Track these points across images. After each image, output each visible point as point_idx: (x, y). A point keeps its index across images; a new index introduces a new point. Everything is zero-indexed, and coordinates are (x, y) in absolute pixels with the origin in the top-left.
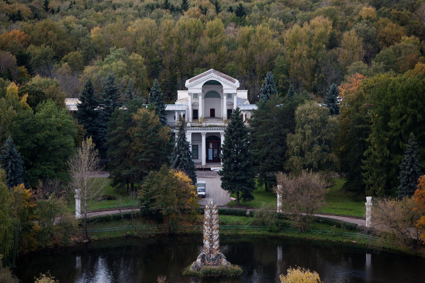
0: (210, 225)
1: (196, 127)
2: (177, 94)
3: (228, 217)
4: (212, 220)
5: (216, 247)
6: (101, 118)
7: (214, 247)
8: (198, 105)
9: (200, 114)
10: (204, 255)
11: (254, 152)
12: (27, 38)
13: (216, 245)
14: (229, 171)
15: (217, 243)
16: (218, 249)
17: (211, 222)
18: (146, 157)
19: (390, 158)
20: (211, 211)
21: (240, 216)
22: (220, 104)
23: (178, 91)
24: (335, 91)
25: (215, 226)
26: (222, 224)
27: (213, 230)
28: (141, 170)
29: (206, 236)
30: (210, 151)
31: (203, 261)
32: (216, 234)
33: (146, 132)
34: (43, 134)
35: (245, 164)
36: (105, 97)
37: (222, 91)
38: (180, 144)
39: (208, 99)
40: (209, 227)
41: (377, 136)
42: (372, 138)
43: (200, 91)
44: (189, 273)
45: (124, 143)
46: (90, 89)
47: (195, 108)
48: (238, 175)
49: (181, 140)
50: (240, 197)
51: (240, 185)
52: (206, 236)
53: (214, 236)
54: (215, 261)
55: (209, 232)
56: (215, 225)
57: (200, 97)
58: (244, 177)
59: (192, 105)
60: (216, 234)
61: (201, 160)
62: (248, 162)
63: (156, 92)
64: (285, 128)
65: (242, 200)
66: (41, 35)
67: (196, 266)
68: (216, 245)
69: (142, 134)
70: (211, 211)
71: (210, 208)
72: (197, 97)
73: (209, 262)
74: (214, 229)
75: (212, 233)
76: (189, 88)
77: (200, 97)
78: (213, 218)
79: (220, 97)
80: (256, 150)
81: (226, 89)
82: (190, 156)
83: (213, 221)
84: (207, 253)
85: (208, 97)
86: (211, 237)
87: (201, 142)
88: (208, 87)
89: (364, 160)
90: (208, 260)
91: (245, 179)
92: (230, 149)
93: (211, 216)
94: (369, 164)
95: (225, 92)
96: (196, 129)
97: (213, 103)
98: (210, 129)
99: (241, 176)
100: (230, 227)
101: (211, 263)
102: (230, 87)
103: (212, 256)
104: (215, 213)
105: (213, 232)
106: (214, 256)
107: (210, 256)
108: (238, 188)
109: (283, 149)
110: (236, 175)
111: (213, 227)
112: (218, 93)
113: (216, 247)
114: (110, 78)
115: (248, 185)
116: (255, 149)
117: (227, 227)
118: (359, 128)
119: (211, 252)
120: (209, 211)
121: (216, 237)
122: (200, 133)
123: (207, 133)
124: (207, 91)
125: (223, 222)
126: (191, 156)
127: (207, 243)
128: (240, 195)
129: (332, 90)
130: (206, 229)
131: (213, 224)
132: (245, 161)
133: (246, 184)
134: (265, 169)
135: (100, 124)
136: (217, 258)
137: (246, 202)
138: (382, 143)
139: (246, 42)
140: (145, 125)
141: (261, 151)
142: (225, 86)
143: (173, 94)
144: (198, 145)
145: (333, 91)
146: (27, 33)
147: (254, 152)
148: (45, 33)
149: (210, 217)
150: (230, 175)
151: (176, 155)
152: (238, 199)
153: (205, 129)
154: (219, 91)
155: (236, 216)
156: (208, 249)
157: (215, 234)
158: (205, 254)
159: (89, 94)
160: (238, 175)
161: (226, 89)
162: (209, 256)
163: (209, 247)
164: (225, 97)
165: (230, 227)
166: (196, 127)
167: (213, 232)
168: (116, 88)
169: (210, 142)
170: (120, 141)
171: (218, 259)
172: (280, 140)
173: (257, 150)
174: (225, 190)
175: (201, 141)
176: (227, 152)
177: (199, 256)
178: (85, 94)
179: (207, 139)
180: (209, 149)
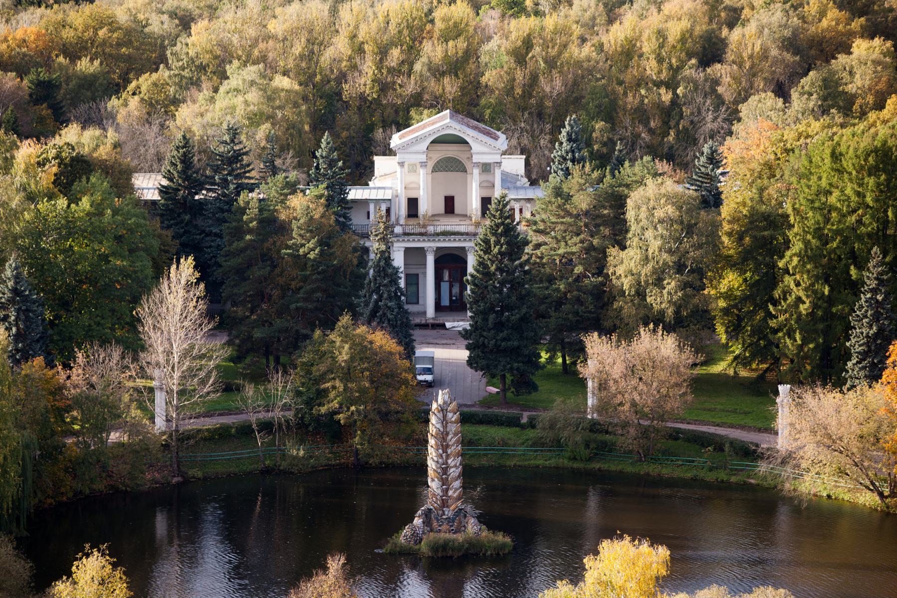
3: (481, 428)
4: (447, 434)
5: (454, 492)
7: (450, 493)
13: (456, 489)
15: (457, 484)
21: (507, 426)
25: (453, 448)
27: (448, 457)
39: (432, 356)
44: (398, 549)
48: (504, 339)
53: (452, 470)
54: (453, 522)
56: (453, 445)
58: (516, 343)
61: (425, 305)
75: (447, 463)
76: (400, 151)
78: (448, 430)
81: (478, 153)
82: (400, 297)
83: (450, 437)
84: (436, 505)
86: (445, 471)
90: (438, 520)
91: (518, 347)
95: (476, 159)
99: (509, 340)
100: (485, 450)
103: (446, 513)
104: (453, 419)
105: (449, 461)
111: (449, 451)
113: (454, 492)
117: (479, 450)
119: (444, 504)
121: (454, 472)
123: (438, 249)
126: (403, 298)
136: (457, 516)
142: (475, 147)
144: (417, 275)
151: (371, 296)
154: (463, 157)
161: (478, 153)
165: (485, 450)
167: (449, 461)
171: (460, 519)
175: (425, 265)
179: (437, 262)
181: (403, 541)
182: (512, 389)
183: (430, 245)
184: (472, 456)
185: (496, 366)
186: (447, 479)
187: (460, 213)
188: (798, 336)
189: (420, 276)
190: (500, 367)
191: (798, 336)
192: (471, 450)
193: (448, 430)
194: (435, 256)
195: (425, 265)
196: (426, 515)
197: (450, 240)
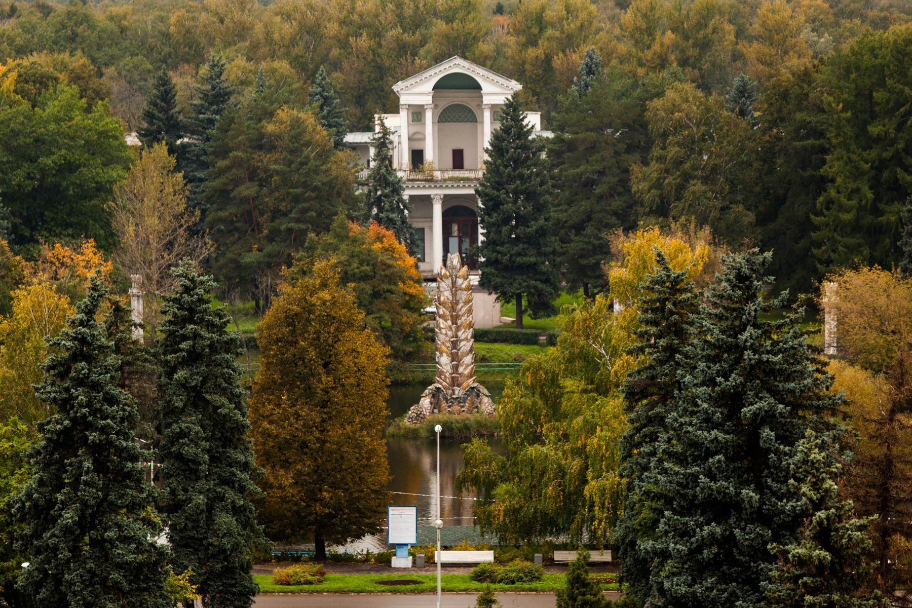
0: (452, 316)
1: (418, 180)
2: (387, 513)
3: (496, 346)
4: (457, 303)
5: (465, 369)
6: (194, 158)
7: (461, 370)
8: (424, 139)
9: (429, 155)
10: (439, 388)
11: (556, 211)
12: (29, 41)
13: (467, 366)
14: (497, 245)
16: (470, 376)
17: (453, 309)
18: (298, 221)
19: (876, 211)
20: (454, 283)
21: (524, 344)
22: (475, 136)
23: (391, 509)
24: (745, 90)
25: (463, 318)
26: (481, 360)
27: (458, 329)
28: (287, 252)
29: (443, 343)
30: (454, 242)
31: (436, 405)
32: (466, 339)
33: (299, 160)
34: (54, 157)
35: (534, 227)
36: (203, 111)
37: (480, 105)
38: (379, 180)
40: (449, 322)
41: (845, 158)
42: (833, 166)
43: (427, 100)
44: (402, 431)
45: (247, 188)
46: (165, 91)
47: (417, 146)
49: (383, 171)
50: (523, 308)
51: (525, 277)
52: (443, 343)
53: (463, 343)
54: (465, 402)
55: (449, 333)
56: (463, 315)
57: (429, 116)
58: (533, 259)
59: (409, 139)
60: (466, 339)
61: (432, 263)
62: (542, 222)
63: (322, 96)
64: (629, 153)
65: (529, 315)
66: (60, 37)
67: (418, 415)
68: (467, 366)
69: (289, 166)
70: (454, 283)
71: (451, 276)
72: (420, 120)
73: (449, 407)
74: (461, 325)
75: (457, 336)
76: (402, 92)
77: (429, 116)
78: (458, 298)
79: (476, 121)
80: (560, 208)
81: (489, 94)
82: (402, 211)
83: (460, 306)
84: (444, 383)
85: (446, 121)
86: (455, 344)
87: (432, 221)
88: (447, 95)
89: (816, 215)
90: (447, 400)
91: (535, 264)
92: (498, 190)
93: (454, 295)
94: (827, 225)
96: (419, 187)
97: (458, 136)
98: (452, 186)
99: (525, 255)
100: (500, 366)
101: (456, 408)
102: (498, 90)
103: (456, 392)
104: (463, 286)
105: (460, 334)
106: (461, 391)
107: (453, 391)
108: (520, 284)
109: (625, 202)
110: (513, 252)
111: (459, 322)
112: (470, 110)
113: (465, 369)
114: (215, 65)
115: (544, 278)
116: (559, 205)
117: (492, 367)
118: (804, 148)
119: (455, 382)
120: (449, 281)
122: (429, 196)
123: (445, 196)
124: (444, 104)
125: (484, 356)
126: (406, 212)
127: (444, 361)
128: (524, 303)
129: (738, 89)
130: (442, 326)
131: (460, 313)
132: (536, 219)
133: (538, 276)
134: (584, 249)
135: (191, 174)
136: (468, 395)
137: (538, 320)
138: (857, 174)
139: (535, 30)
140: (296, 145)
141: (574, 208)
143: (381, 509)
144: (423, 230)
145: (741, 92)
146: (28, 32)
147: (556, 211)
148: (70, 32)
149: (450, 298)
150: (499, 252)
151: (370, 209)
152: (520, 313)
153: (441, 187)
154: (472, 105)
155: (514, 343)
156: (447, 375)
157: (463, 337)
158: (440, 386)
159: (163, 104)
160: (519, 254)
161: (489, 94)
162: (450, 392)
163: (450, 371)
164: (487, 115)
165: (500, 366)
166: (418, 180)
167: (460, 334)
168: (228, 90)
169: (453, 221)
170: (237, 182)
171: (472, 399)
172: (620, 181)
173: (564, 207)
174: (490, 294)
175: (431, 217)
176: (492, 199)
177: (427, 391)
178: (155, 105)
179: (445, 215)
180: (451, 239)
181: (408, 423)
182: (530, 312)
183: (437, 193)
184: (486, 373)
185: (511, 284)
186: (457, 354)
187: (464, 597)
188: (841, 105)
189: (427, 231)
190: (515, 285)
191: (841, 105)
192: (483, 366)
193: (458, 298)
194: (443, 206)
195: (432, 217)
196: (433, 396)
197: (458, 186)
